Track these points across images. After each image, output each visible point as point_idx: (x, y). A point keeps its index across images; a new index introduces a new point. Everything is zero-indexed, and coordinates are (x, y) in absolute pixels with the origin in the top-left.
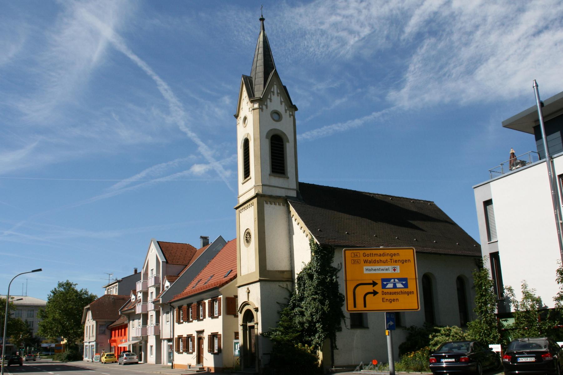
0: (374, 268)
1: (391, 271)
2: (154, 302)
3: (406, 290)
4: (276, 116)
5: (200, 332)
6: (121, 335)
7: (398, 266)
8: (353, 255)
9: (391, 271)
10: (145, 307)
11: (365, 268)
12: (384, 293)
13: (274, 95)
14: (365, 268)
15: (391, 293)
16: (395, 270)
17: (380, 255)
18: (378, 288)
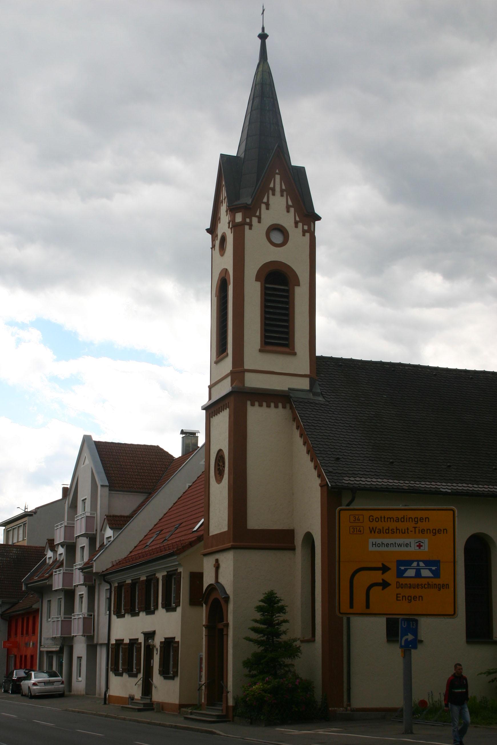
0: (386, 541)
1: (413, 548)
2: (81, 569)
3: (436, 581)
4: (277, 238)
5: (150, 635)
6: (27, 633)
7: (426, 541)
8: (352, 519)
9: (413, 548)
10: (68, 577)
11: (371, 541)
12: (400, 586)
13: (274, 194)
14: (371, 541)
15: (410, 586)
16: (420, 546)
17: (398, 520)
18: (390, 577)
